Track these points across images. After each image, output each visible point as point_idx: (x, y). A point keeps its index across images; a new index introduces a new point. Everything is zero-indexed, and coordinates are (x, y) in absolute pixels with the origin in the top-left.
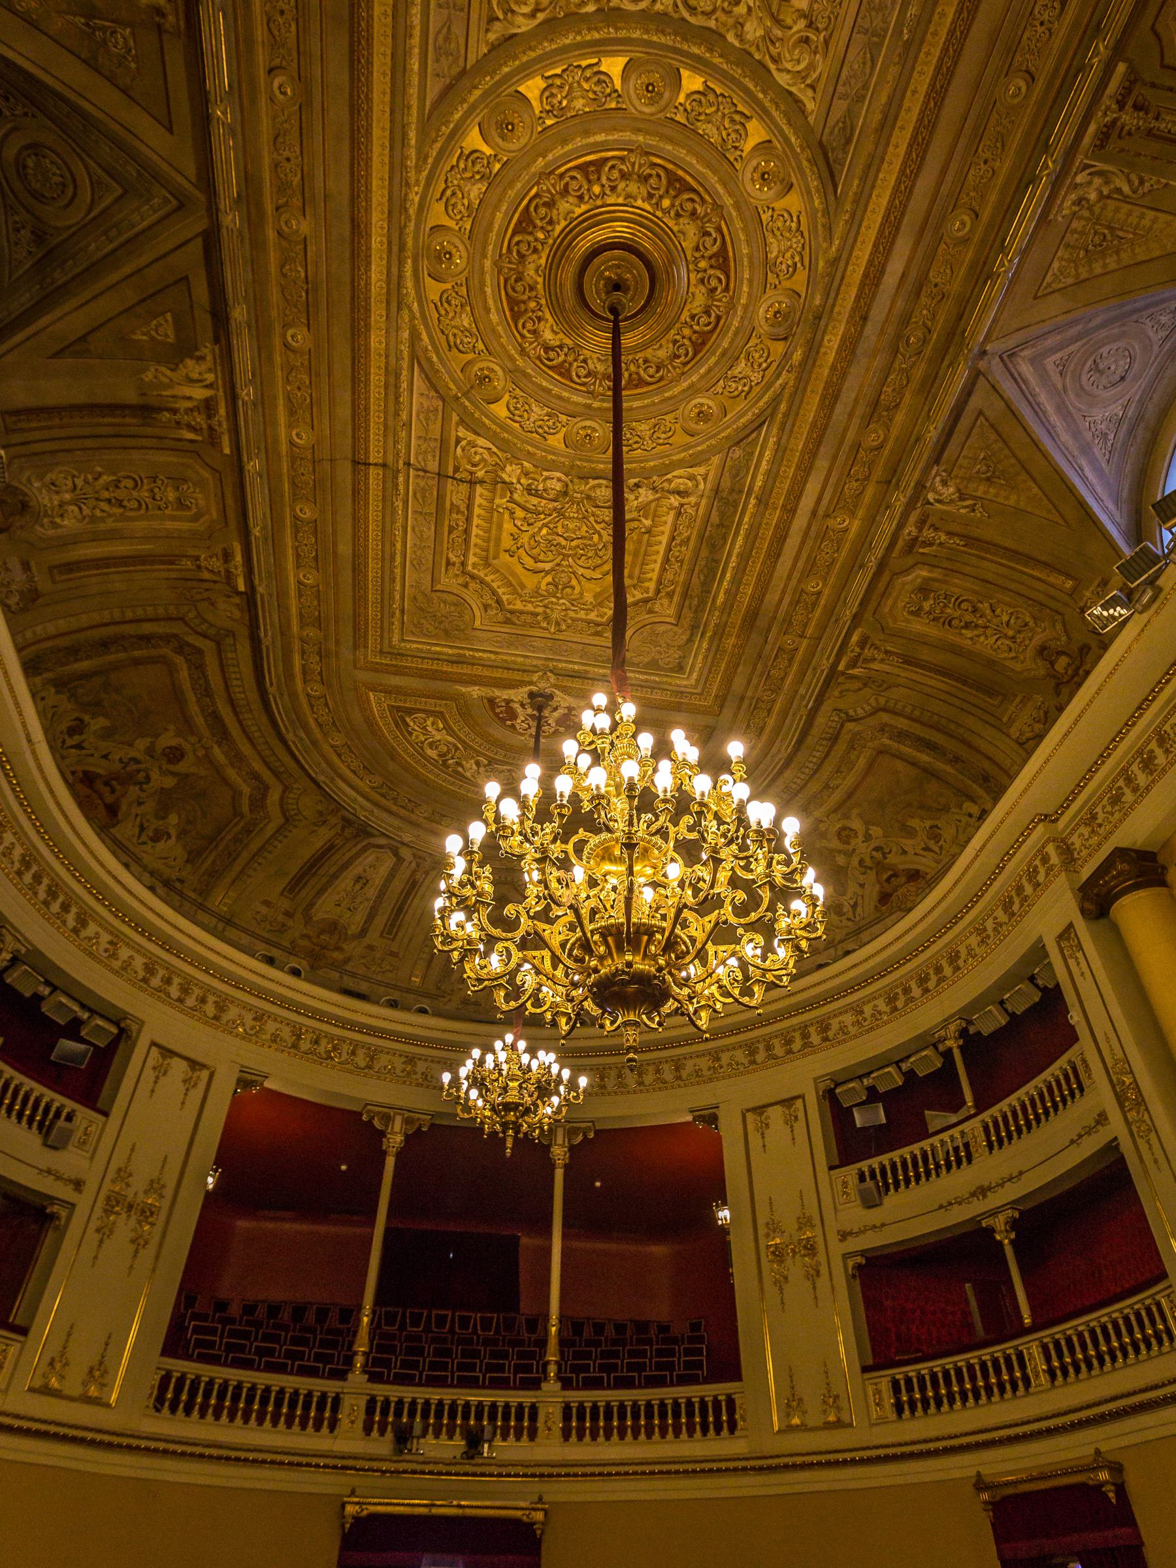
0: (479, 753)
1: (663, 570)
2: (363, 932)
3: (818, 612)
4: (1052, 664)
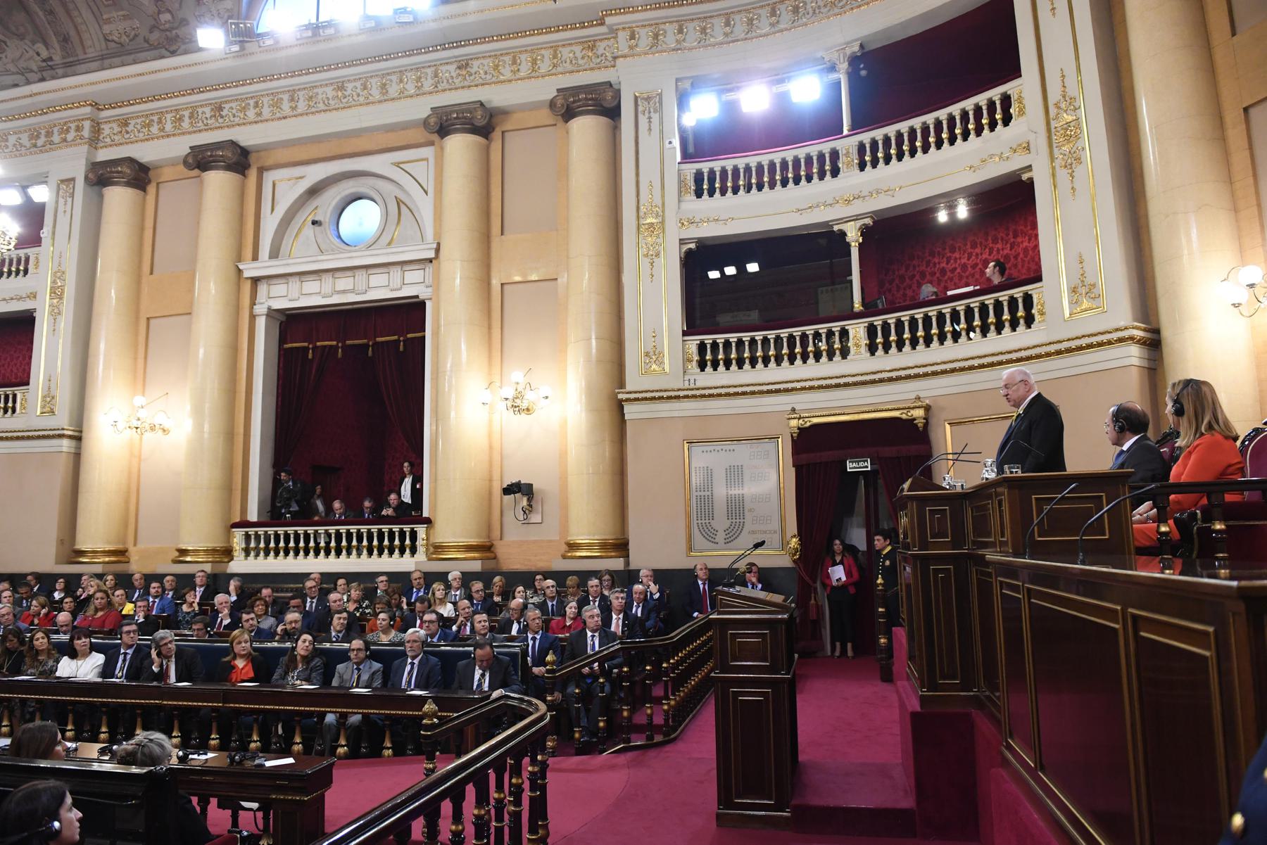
4: (159, 12)
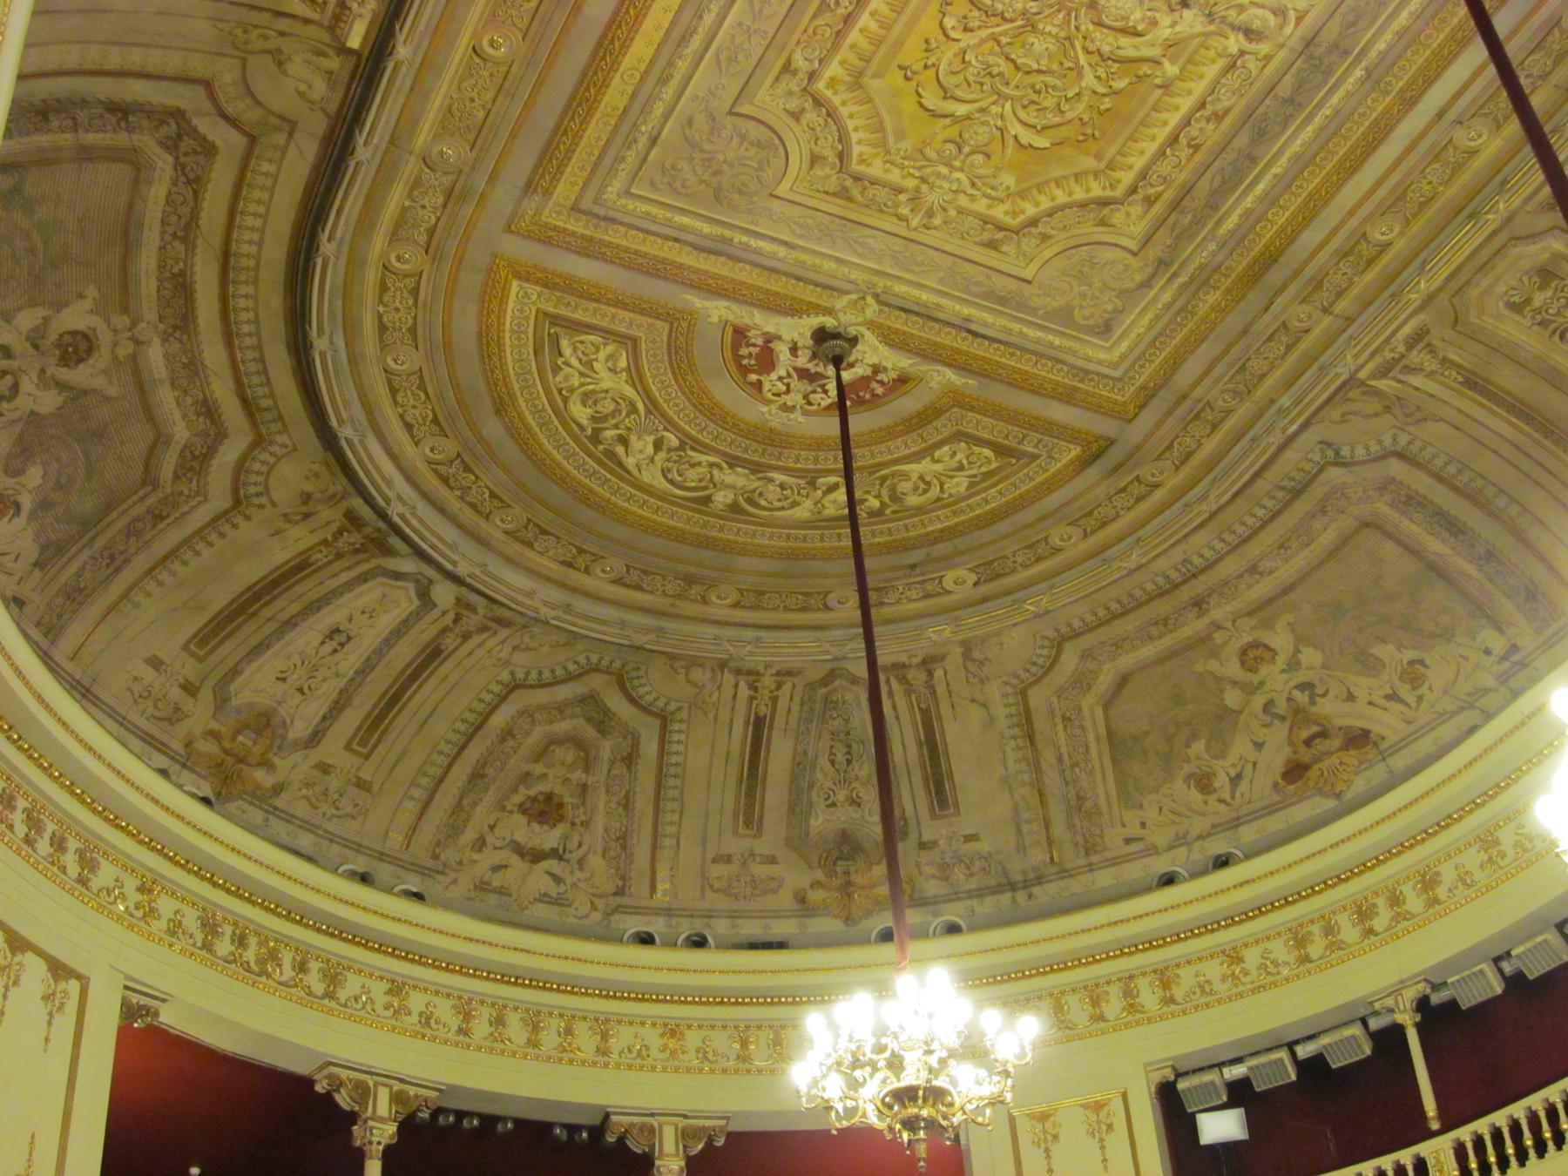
0: (670, 424)
1: (1161, 154)
2: (315, 738)
3: (1370, 276)
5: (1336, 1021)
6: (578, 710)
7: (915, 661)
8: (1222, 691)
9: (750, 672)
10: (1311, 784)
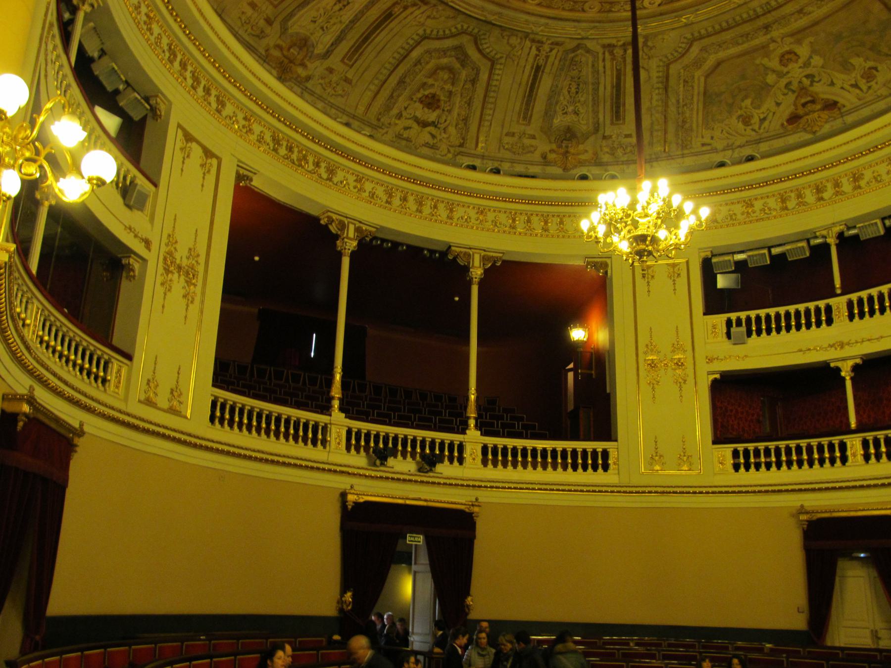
2: (327, 54)
5: (792, 239)
6: (453, 53)
7: (620, 43)
8: (767, 74)
9: (539, 42)
10: (801, 126)
